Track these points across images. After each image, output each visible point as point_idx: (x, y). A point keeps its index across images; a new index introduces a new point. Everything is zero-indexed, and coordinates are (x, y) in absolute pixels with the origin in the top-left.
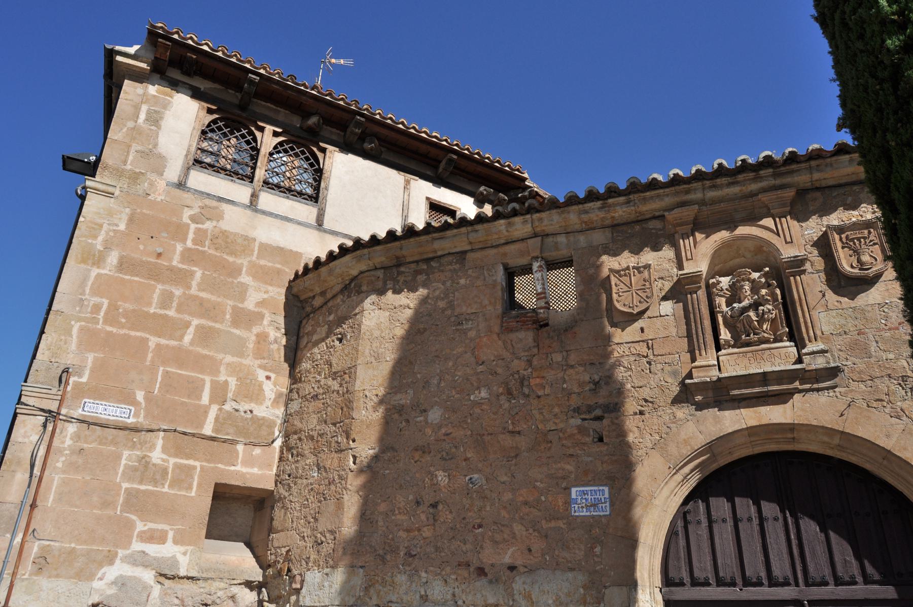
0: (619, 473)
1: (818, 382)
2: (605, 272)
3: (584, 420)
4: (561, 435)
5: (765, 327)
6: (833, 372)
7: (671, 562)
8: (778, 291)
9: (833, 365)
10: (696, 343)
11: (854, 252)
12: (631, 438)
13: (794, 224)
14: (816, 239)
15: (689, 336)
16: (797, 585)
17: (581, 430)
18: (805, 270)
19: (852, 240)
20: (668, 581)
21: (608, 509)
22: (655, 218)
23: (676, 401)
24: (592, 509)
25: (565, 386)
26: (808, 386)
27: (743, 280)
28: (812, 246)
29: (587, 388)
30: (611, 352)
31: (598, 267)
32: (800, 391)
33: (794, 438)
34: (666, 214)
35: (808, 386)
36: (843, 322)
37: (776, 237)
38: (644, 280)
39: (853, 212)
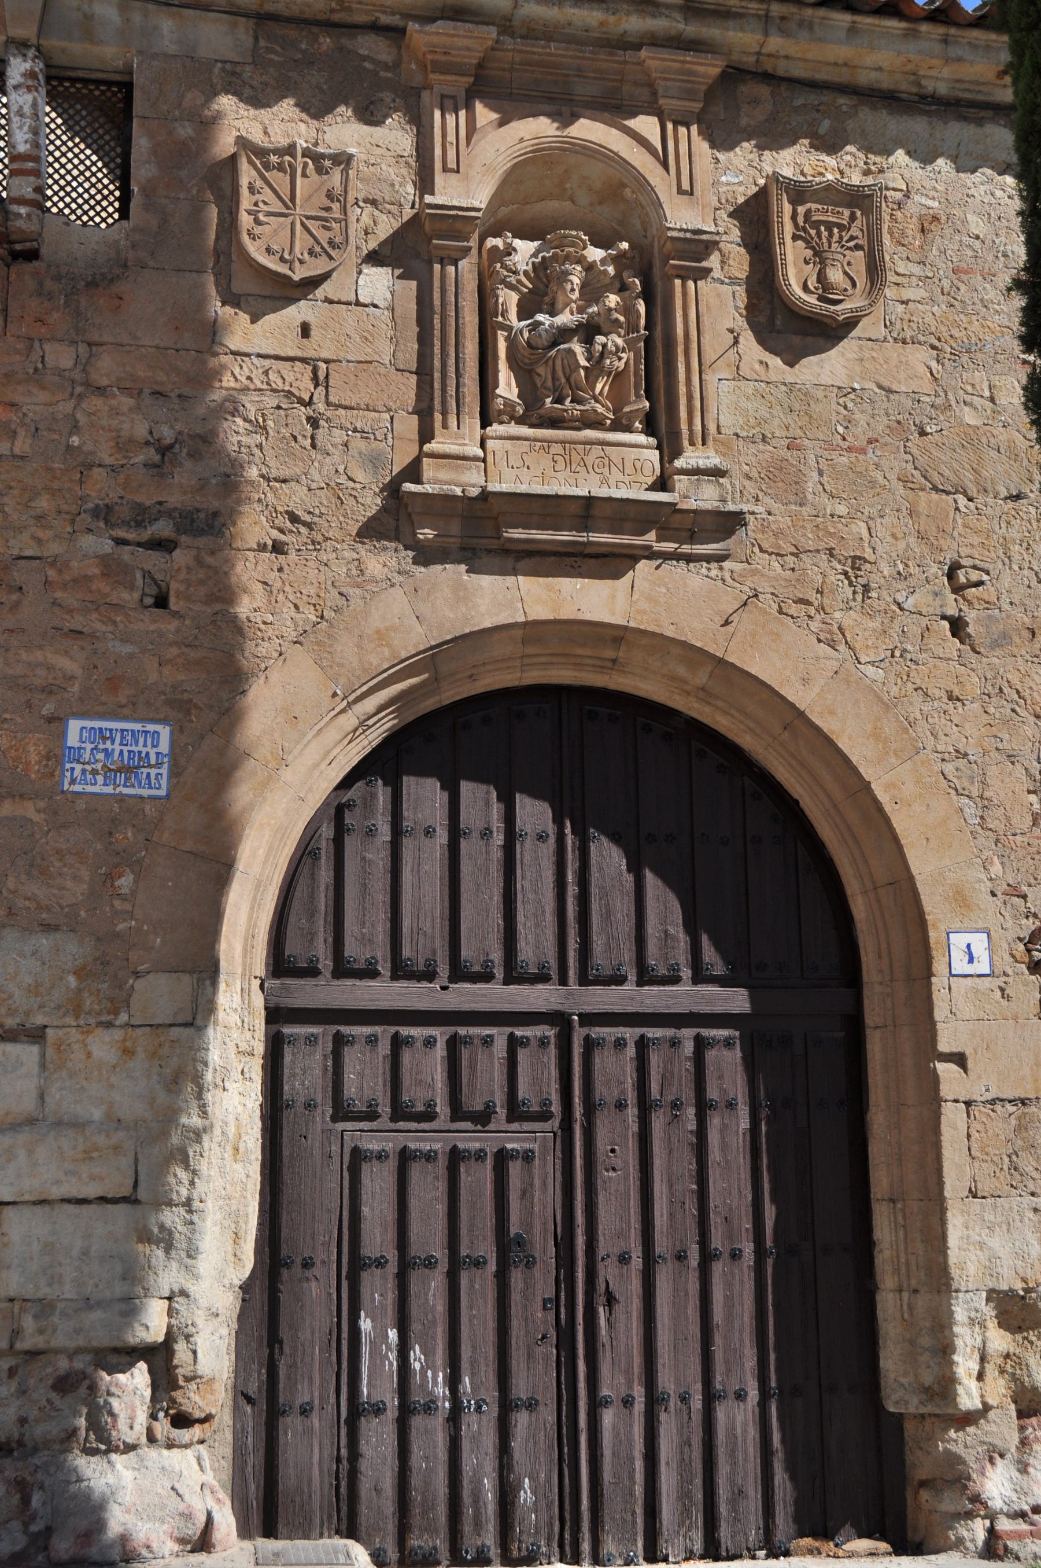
0: (207, 698)
1: (692, 539)
2: (225, 144)
3: (120, 542)
4: (51, 573)
5: (599, 387)
6: (728, 523)
7: (293, 919)
8: (641, 307)
9: (731, 507)
10: (437, 393)
11: (816, 254)
12: (244, 609)
13: (702, 146)
14: (741, 200)
15: (423, 371)
16: (563, 981)
17: (109, 567)
18: (710, 270)
19: (816, 225)
20: (281, 964)
21: (164, 783)
22: (375, 28)
23: (371, 531)
24: (121, 778)
25: (75, 440)
26: (669, 546)
27: (567, 258)
28: (730, 215)
29: (140, 458)
30: (216, 374)
31: (208, 125)
32: (651, 554)
33: (614, 661)
34: (413, 27)
35: (669, 546)
36: (764, 412)
37: (660, 169)
38: (330, 195)
39: (827, 159)
